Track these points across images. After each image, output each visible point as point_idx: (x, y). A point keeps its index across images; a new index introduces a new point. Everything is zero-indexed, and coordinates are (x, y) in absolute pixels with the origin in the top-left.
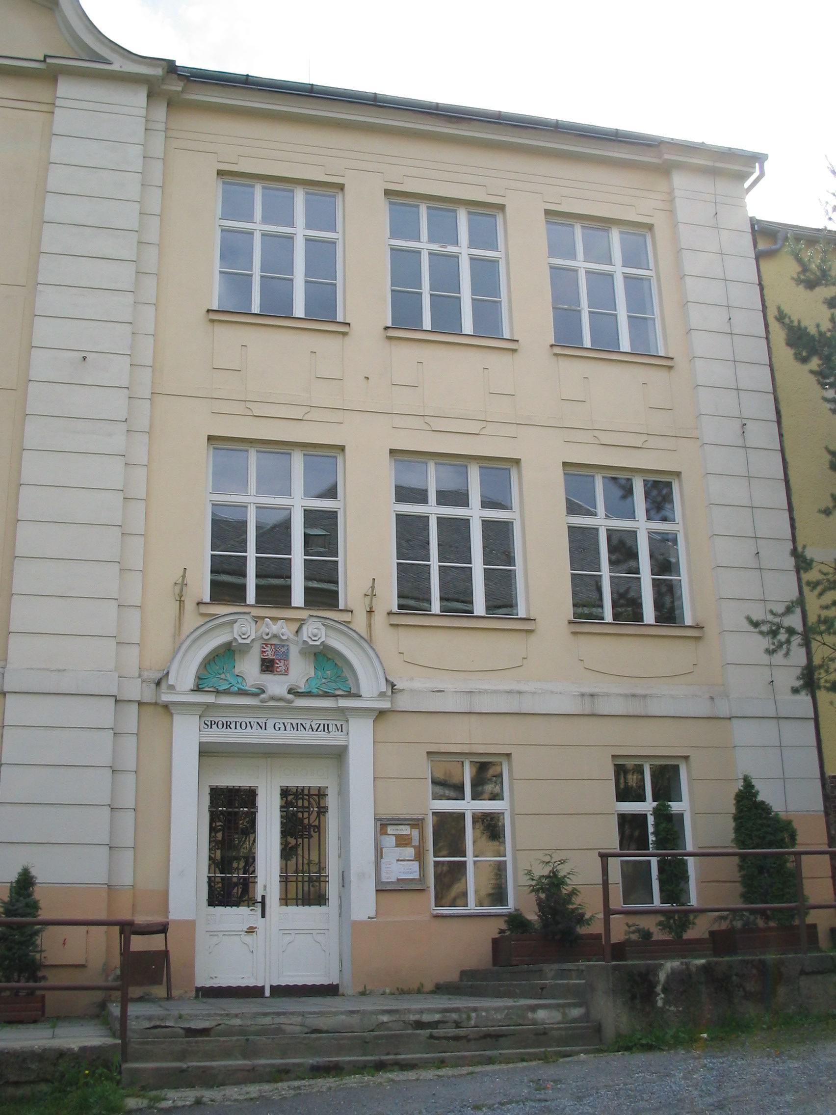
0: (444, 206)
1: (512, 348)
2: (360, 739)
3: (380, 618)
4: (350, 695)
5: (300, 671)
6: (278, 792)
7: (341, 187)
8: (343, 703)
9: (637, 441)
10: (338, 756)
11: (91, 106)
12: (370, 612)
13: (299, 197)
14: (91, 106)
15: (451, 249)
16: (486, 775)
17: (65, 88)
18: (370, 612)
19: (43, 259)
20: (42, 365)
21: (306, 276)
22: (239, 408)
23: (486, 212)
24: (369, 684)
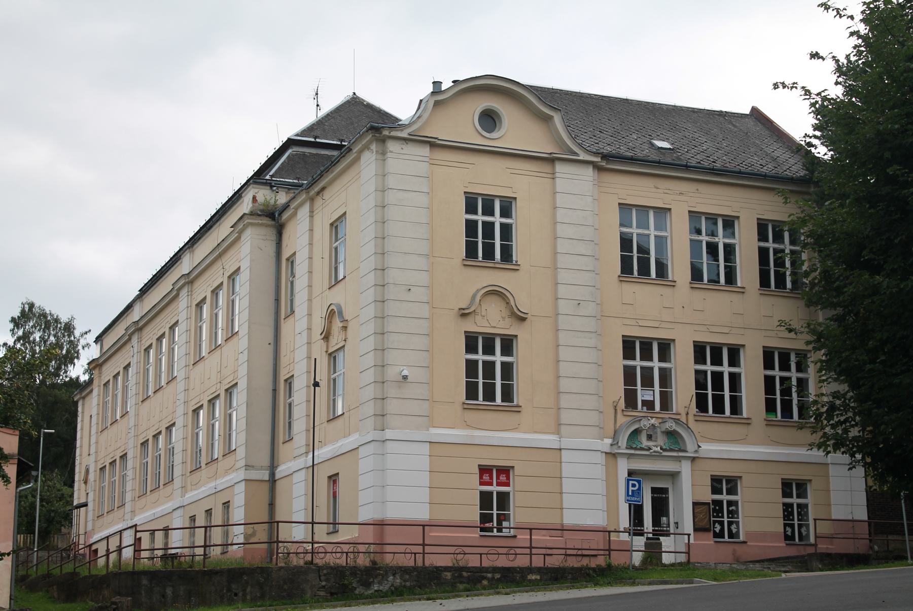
0: (643, 209)
1: (673, 285)
2: (685, 469)
3: (691, 418)
4: (680, 450)
5: (661, 440)
6: (709, 482)
7: (670, 209)
8: (681, 454)
9: (726, 330)
10: (674, 476)
11: (570, 176)
12: (687, 414)
13: (651, 214)
14: (570, 176)
15: (646, 232)
16: (732, 484)
17: (560, 168)
18: (687, 414)
19: (559, 256)
20: (563, 306)
21: (692, 257)
22: (633, 322)
23: (662, 212)
24: (690, 446)
